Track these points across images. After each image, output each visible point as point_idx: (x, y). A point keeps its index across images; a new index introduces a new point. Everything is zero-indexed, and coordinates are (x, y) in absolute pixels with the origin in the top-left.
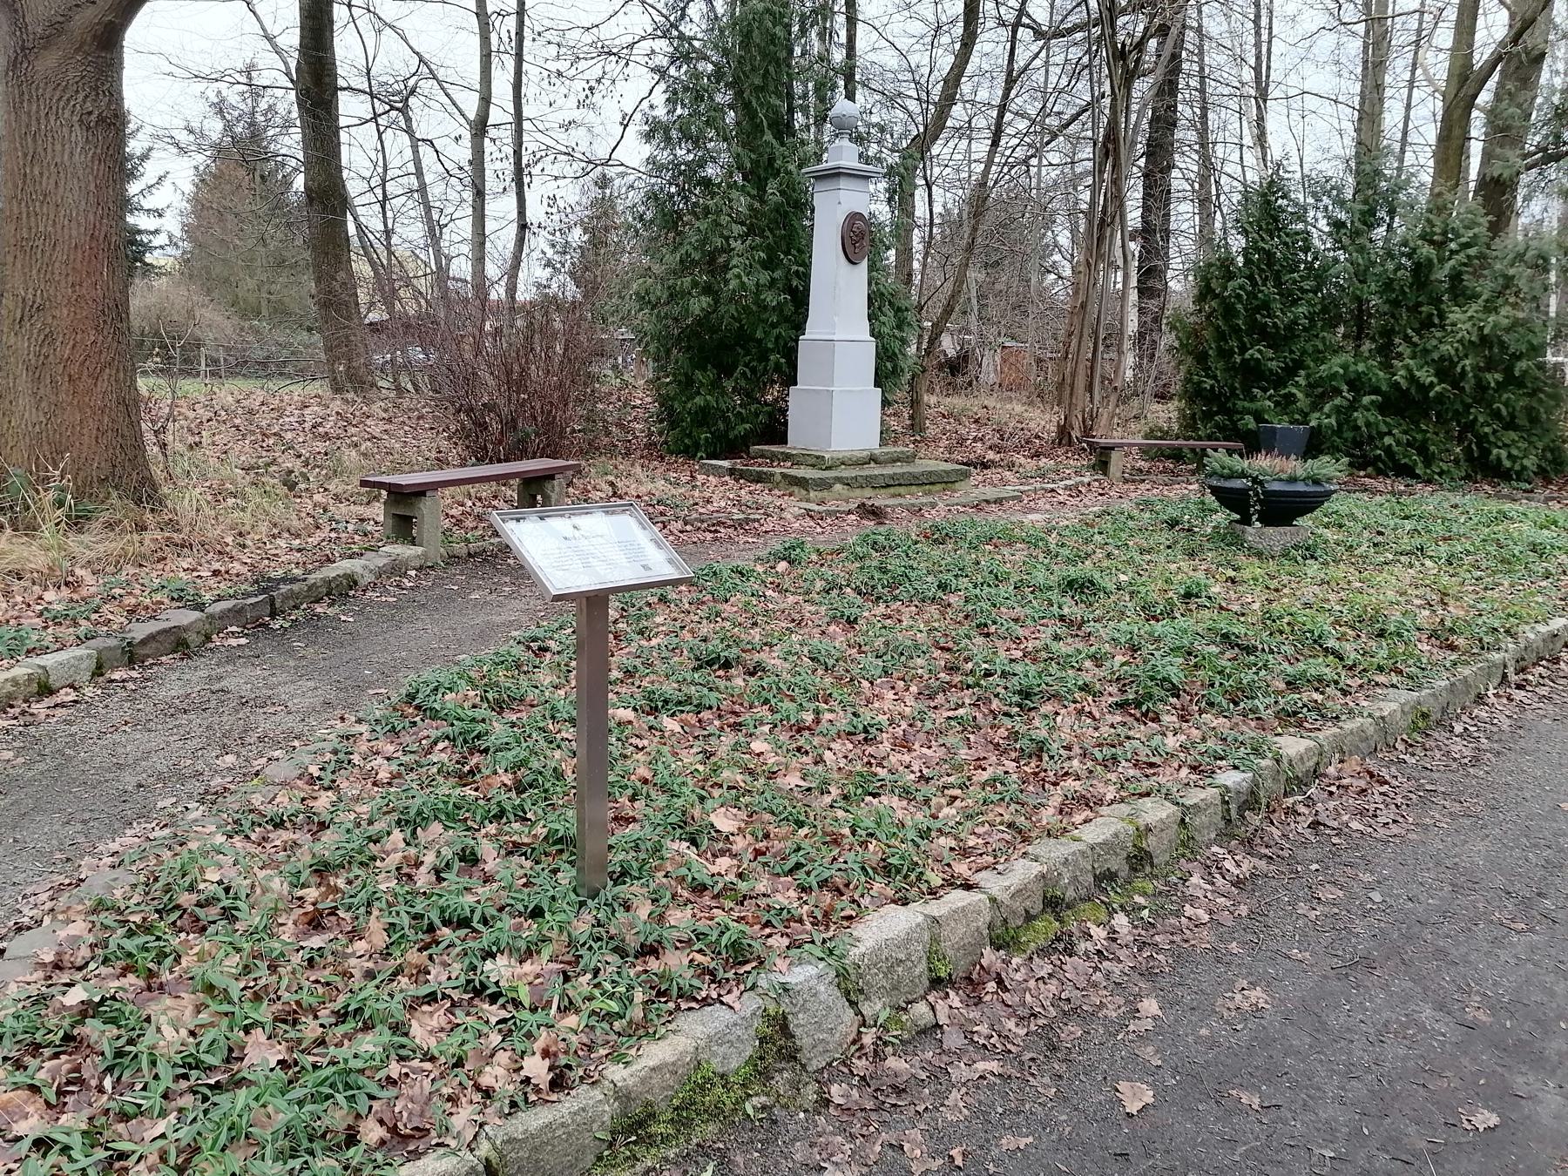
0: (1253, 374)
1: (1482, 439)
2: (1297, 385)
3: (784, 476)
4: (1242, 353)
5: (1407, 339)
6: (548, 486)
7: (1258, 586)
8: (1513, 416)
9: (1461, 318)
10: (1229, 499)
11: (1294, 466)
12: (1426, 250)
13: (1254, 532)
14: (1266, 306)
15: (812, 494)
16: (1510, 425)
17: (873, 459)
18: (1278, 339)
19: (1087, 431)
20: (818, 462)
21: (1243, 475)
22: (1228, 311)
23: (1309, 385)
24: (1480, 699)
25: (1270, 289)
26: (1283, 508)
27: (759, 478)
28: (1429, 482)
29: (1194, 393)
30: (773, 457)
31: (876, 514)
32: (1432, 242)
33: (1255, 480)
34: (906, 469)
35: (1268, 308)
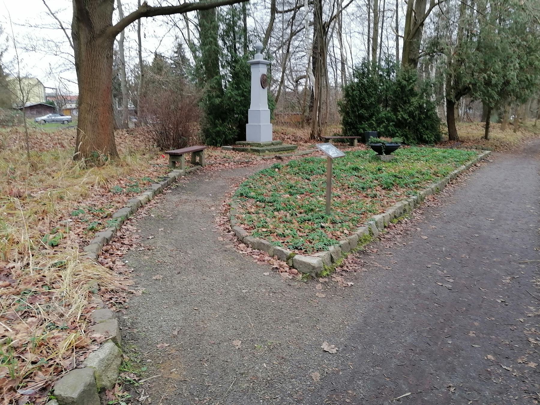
0: (361, 118)
1: (421, 133)
2: (373, 120)
3: (251, 149)
4: (358, 112)
5: (401, 107)
6: (201, 153)
7: (389, 167)
8: (428, 127)
9: (413, 100)
10: (375, 148)
11: (389, 140)
12: (404, 83)
13: (384, 157)
14: (364, 99)
15: (261, 154)
16: (427, 129)
17: (272, 144)
18: (367, 108)
19: (319, 135)
20: (259, 145)
21: (380, 142)
22: (354, 100)
23: (376, 120)
24: (446, 186)
25: (364, 93)
26: (389, 150)
27: (243, 150)
28: (408, 145)
29: (345, 123)
30: (244, 144)
31: (280, 158)
32: (405, 80)
33: (383, 143)
34: (281, 147)
35: (364, 99)
